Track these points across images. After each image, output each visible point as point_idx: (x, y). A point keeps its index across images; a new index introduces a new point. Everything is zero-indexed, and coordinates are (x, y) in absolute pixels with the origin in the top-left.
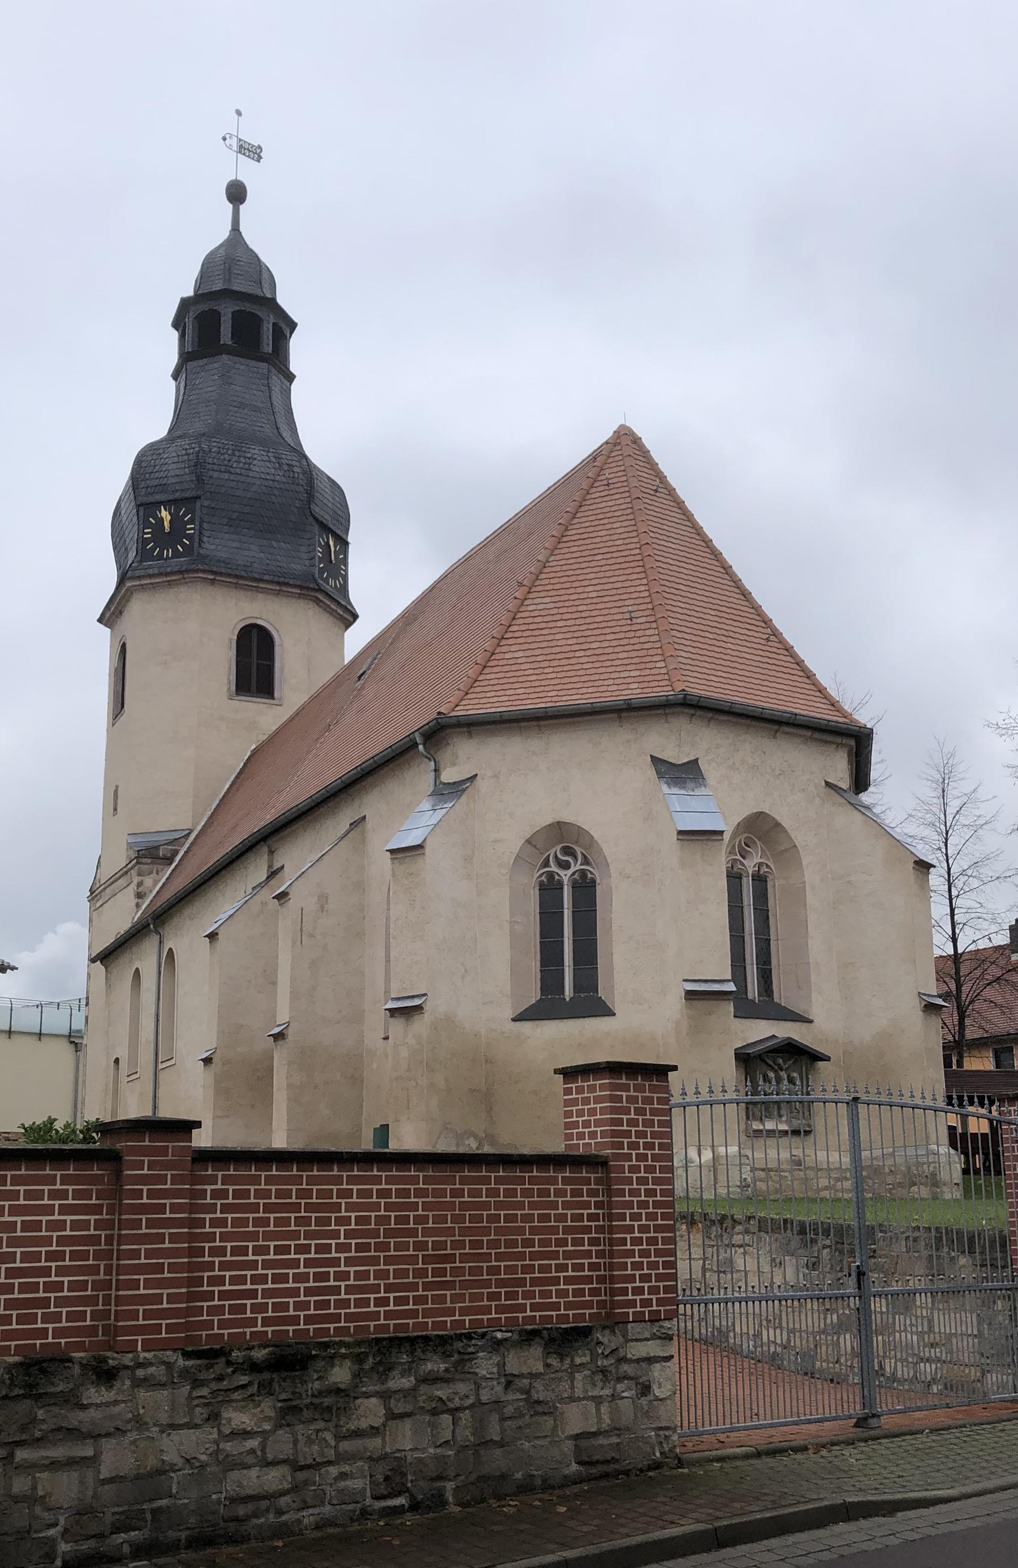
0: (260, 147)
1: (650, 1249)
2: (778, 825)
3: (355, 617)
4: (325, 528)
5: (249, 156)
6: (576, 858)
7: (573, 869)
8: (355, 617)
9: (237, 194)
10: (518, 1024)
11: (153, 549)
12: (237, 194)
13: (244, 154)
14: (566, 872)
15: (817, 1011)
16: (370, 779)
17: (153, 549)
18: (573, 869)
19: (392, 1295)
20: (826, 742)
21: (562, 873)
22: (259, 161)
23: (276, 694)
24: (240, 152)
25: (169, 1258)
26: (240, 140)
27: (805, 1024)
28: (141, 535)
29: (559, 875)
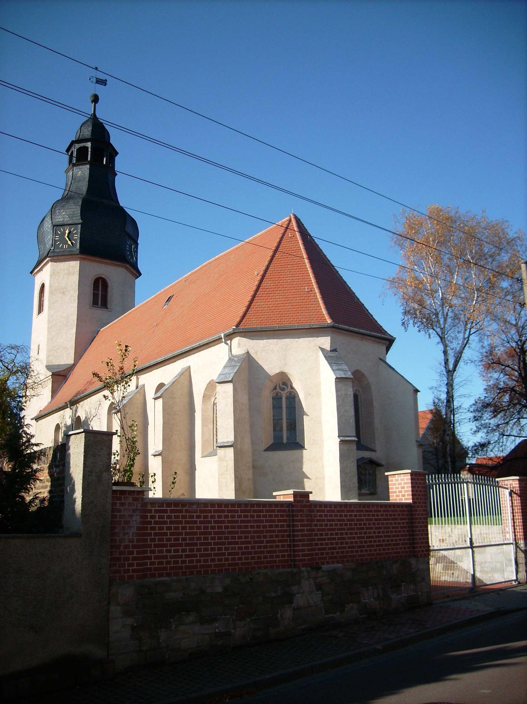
0: (106, 80)
1: (150, 530)
2: (363, 374)
3: (140, 274)
4: (130, 236)
5: (101, 84)
6: (287, 387)
7: (286, 391)
8: (140, 274)
9: (96, 99)
10: (266, 452)
11: (59, 244)
12: (96, 99)
13: (99, 84)
14: (284, 392)
15: (378, 447)
16: (195, 351)
17: (59, 244)
18: (286, 391)
19: (202, 559)
20: (380, 343)
21: (282, 392)
22: (105, 85)
23: (109, 306)
24: (97, 83)
25: (158, 548)
26: (97, 78)
27: (374, 452)
28: (54, 238)
29: (281, 393)
